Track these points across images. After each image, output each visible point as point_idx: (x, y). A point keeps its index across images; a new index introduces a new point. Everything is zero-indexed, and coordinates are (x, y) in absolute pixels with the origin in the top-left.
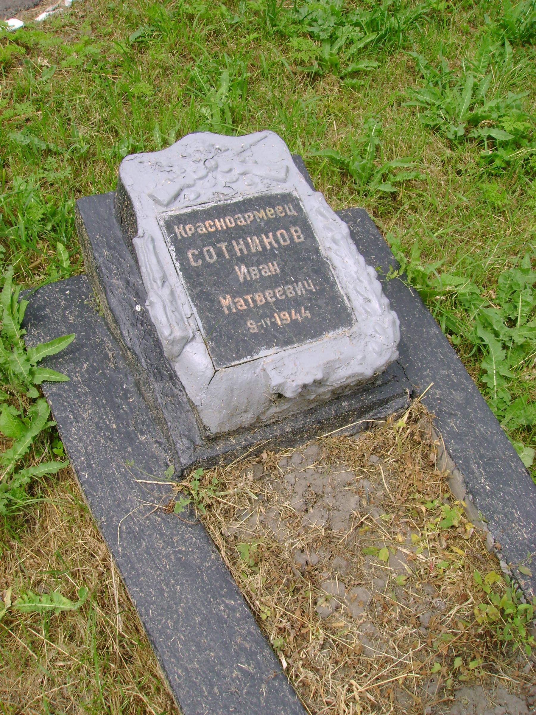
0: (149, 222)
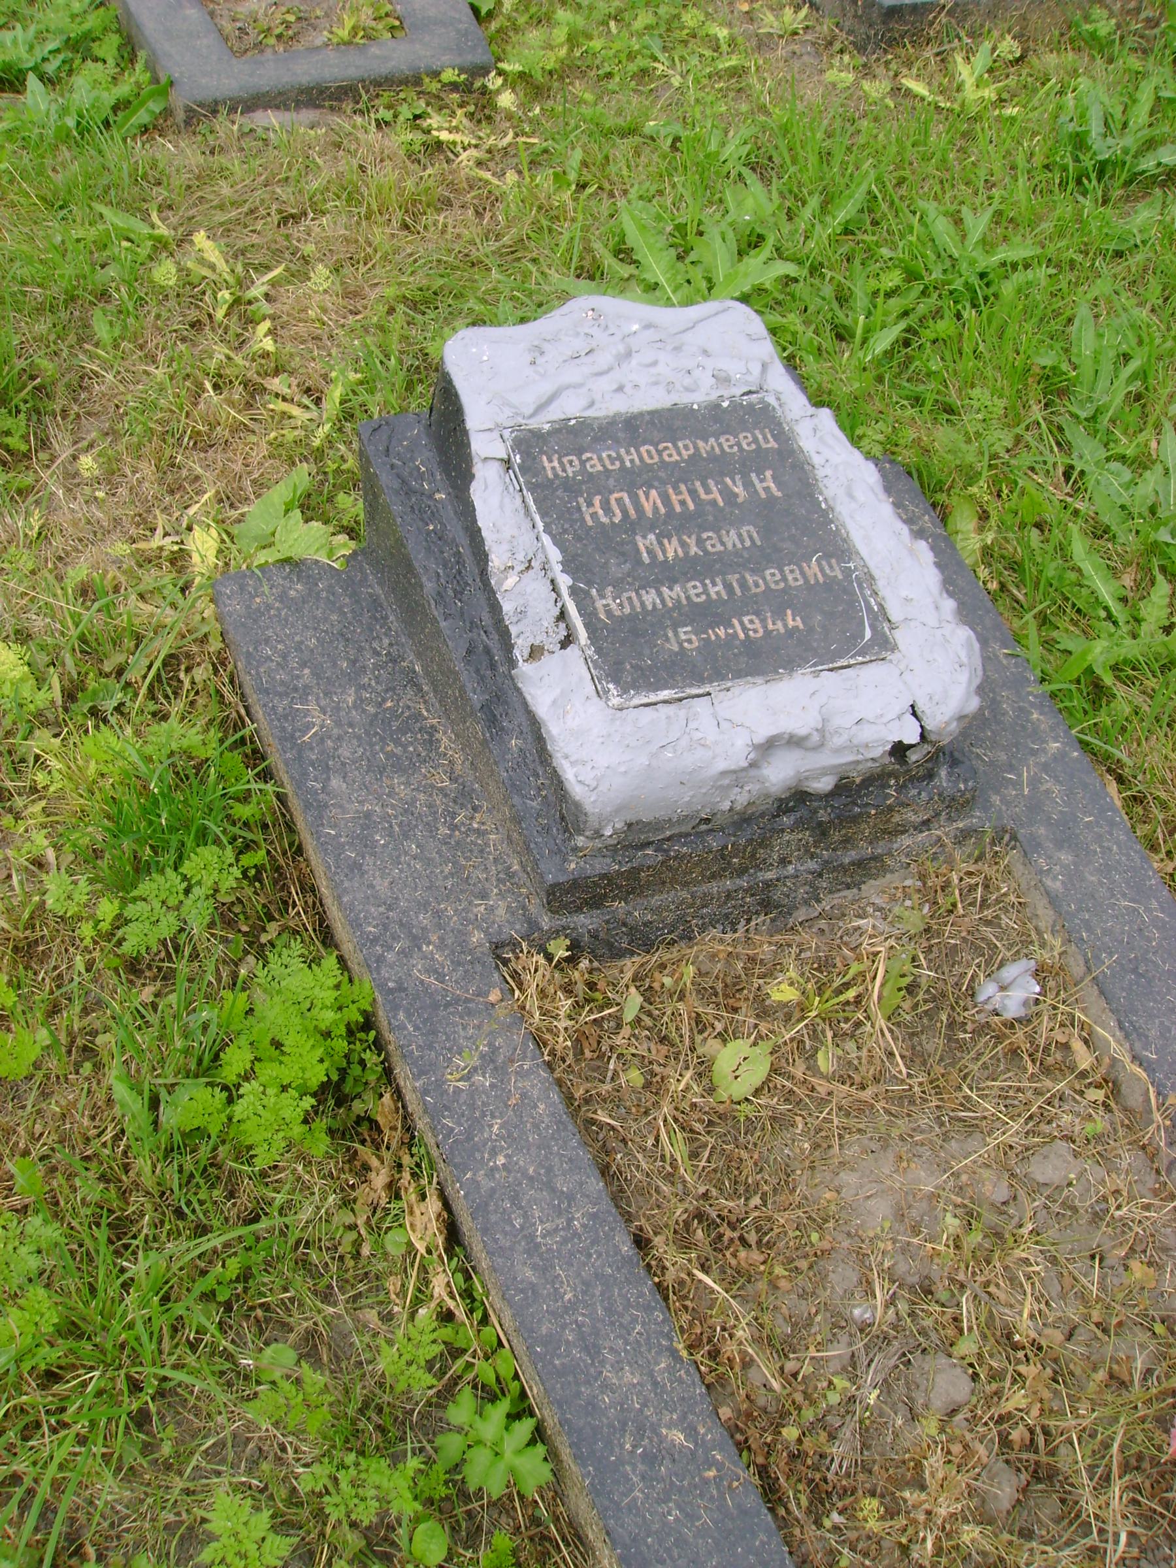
0: (486, 444)
